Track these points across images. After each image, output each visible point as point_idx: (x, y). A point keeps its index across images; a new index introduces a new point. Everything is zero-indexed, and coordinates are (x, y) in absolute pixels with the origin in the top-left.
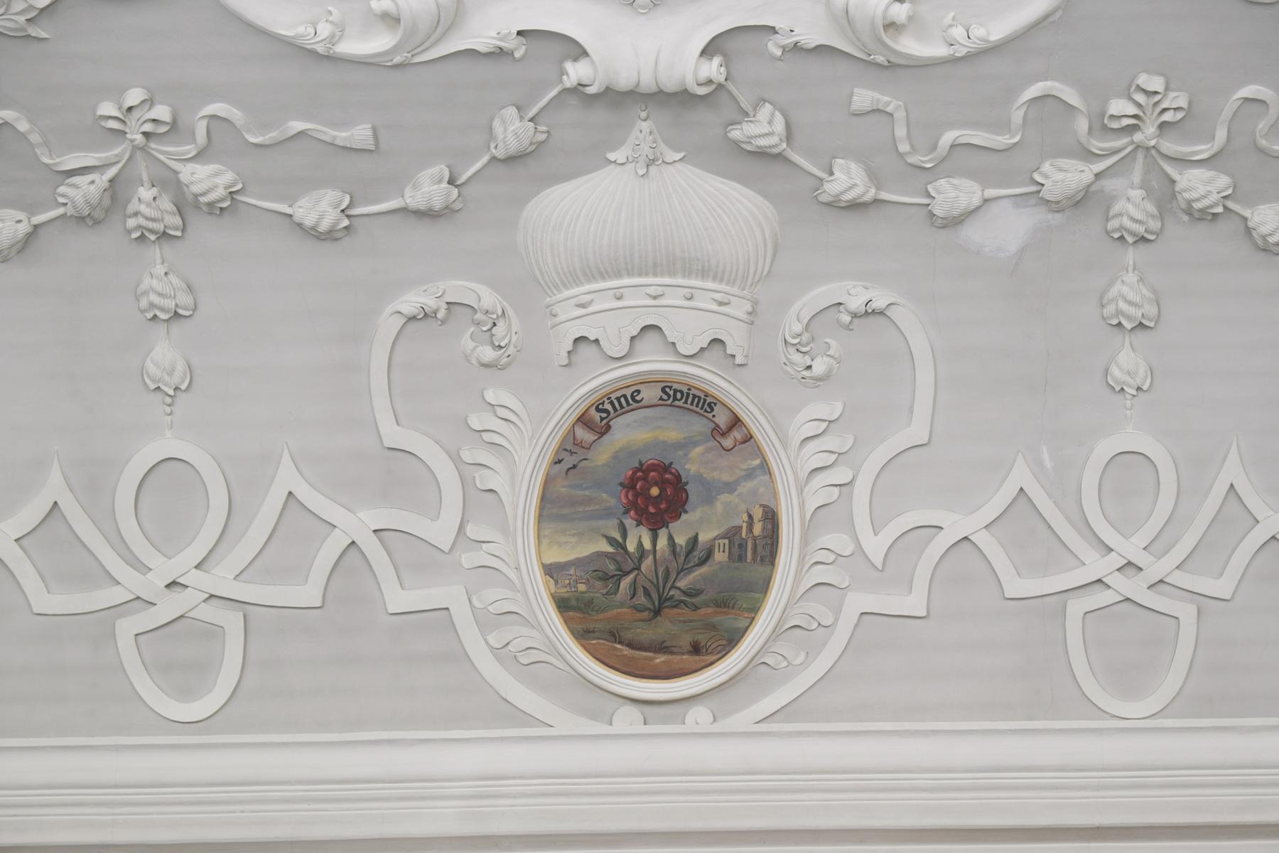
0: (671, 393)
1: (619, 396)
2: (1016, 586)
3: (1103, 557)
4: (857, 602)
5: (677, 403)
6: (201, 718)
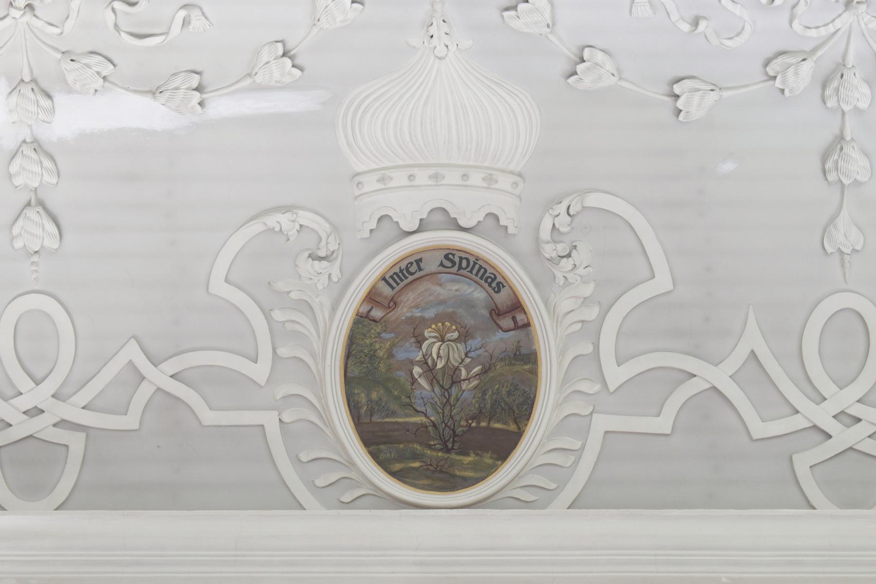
0: (457, 260)
1: (392, 274)
2: (759, 429)
3: (848, 427)
4: (602, 423)
5: (462, 272)
6: (19, 298)
